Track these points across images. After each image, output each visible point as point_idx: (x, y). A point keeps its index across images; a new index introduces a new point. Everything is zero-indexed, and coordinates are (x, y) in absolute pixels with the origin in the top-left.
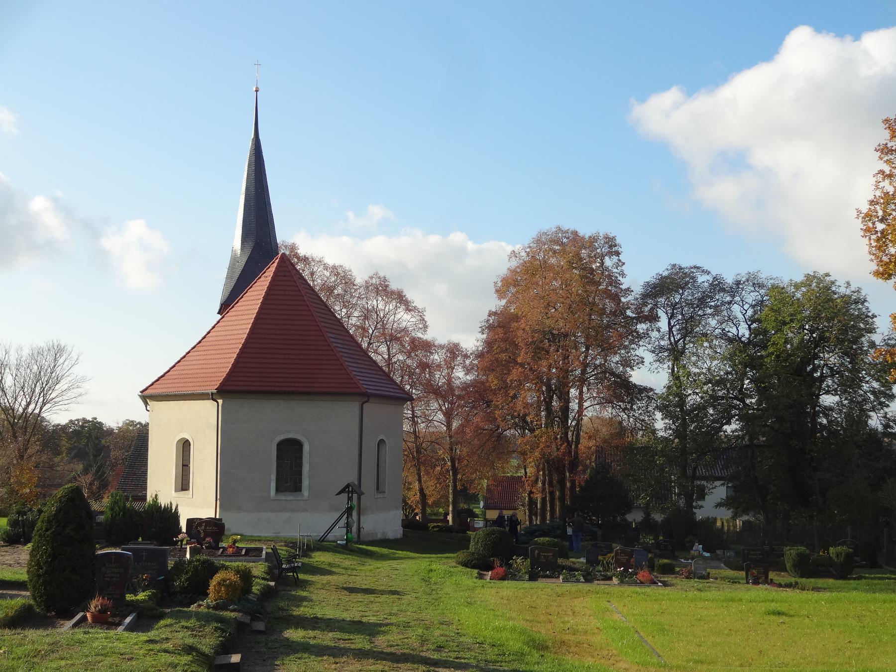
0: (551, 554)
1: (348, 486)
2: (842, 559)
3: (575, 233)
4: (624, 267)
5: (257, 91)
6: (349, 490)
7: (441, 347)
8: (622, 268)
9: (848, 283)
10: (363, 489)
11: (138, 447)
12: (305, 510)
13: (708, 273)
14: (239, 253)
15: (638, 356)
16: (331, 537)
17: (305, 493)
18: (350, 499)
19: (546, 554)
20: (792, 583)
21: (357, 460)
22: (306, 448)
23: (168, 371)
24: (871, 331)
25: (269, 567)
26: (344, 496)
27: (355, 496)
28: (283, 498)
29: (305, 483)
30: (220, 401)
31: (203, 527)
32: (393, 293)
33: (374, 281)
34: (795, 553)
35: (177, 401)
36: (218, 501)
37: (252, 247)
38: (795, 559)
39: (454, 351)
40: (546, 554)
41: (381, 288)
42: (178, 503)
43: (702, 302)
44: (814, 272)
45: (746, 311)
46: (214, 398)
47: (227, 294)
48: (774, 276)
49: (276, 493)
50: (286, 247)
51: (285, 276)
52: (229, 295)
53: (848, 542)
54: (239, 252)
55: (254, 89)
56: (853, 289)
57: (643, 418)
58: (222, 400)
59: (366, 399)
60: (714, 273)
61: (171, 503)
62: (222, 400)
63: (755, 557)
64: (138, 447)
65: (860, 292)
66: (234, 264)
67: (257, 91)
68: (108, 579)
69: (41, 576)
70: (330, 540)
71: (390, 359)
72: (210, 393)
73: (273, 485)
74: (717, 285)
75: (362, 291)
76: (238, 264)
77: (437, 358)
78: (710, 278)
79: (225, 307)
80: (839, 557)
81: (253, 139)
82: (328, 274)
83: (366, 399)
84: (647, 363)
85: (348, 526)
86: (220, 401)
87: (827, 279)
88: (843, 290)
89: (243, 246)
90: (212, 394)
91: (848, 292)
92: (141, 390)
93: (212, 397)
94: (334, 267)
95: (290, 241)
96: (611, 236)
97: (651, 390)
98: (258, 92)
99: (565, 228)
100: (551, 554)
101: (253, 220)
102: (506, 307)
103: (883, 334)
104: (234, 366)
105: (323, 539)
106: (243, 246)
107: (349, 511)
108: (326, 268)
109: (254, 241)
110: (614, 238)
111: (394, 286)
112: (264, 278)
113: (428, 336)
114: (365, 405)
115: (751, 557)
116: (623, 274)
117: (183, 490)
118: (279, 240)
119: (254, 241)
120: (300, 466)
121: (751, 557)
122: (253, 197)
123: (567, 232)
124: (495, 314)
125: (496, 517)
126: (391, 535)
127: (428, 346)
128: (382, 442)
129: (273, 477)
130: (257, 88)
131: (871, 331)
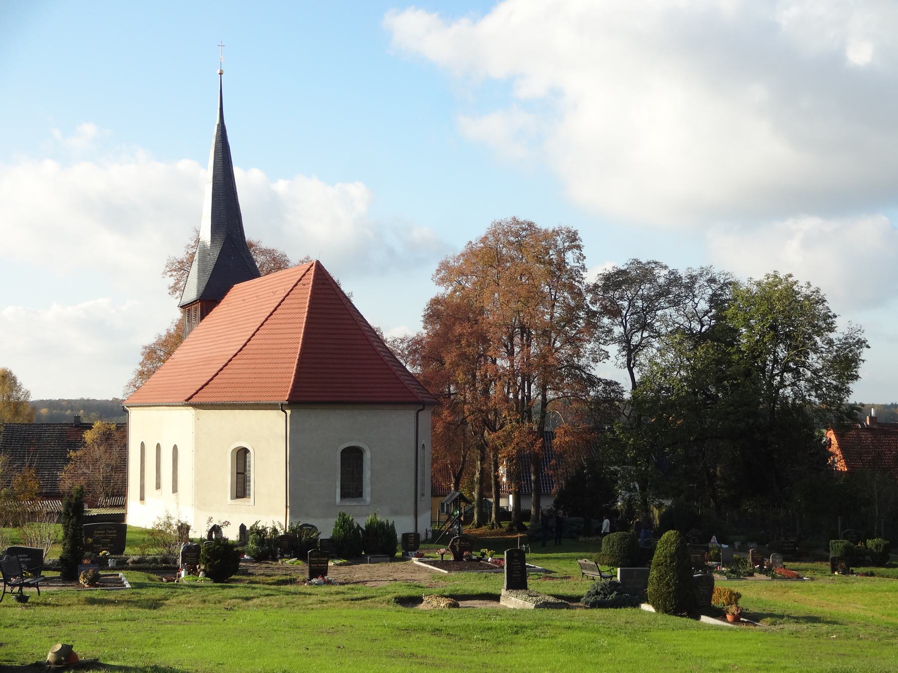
0: (700, 555)
2: (881, 550)
3: (531, 225)
4: (585, 262)
5: (221, 74)
8: (584, 262)
9: (809, 283)
11: (7, 439)
13: (666, 267)
14: (209, 245)
15: (603, 350)
19: (695, 556)
20: (868, 572)
22: (367, 456)
23: (212, 379)
24: (831, 330)
28: (348, 504)
29: (367, 489)
30: (288, 412)
31: (458, 542)
34: (842, 546)
35: (209, 410)
36: (288, 508)
37: (224, 240)
38: (843, 550)
40: (695, 556)
42: (173, 496)
43: (663, 292)
44: (775, 272)
45: (697, 304)
46: (283, 408)
47: (202, 288)
48: (726, 272)
49: (341, 500)
51: (323, 284)
52: (205, 289)
53: (852, 532)
54: (209, 243)
55: (219, 72)
56: (812, 289)
57: (609, 411)
58: (290, 411)
59: (421, 407)
60: (671, 268)
61: (387, 520)
62: (290, 411)
63: (788, 548)
64: (7, 439)
65: (818, 292)
66: (204, 257)
67: (221, 74)
68: (702, 593)
69: (671, 592)
72: (280, 404)
73: (338, 491)
74: (674, 280)
76: (209, 257)
78: (666, 272)
80: (878, 548)
81: (218, 125)
83: (421, 407)
84: (612, 358)
86: (288, 412)
87: (790, 279)
88: (805, 291)
89: (213, 238)
90: (282, 405)
91: (808, 293)
92: (186, 398)
93: (282, 408)
96: (573, 230)
97: (616, 383)
98: (222, 75)
99: (521, 220)
100: (700, 555)
101: (224, 211)
102: (451, 296)
103: (843, 333)
106: (213, 238)
109: (225, 233)
110: (575, 233)
112: (302, 286)
114: (420, 413)
115: (784, 548)
116: (584, 268)
117: (237, 497)
119: (225, 233)
121: (784, 548)
122: (221, 187)
123: (522, 223)
125: (34, 397)
129: (338, 484)
130: (221, 70)
131: (831, 330)
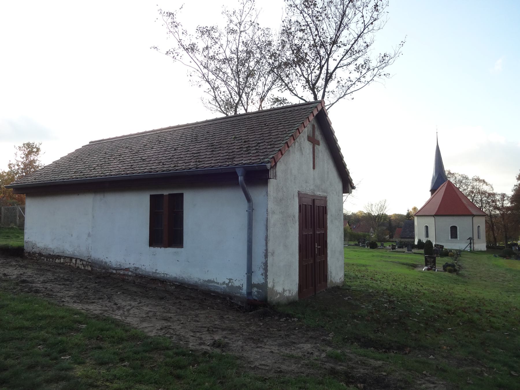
1: (470, 238)
6: (470, 239)
7: (499, 194)
10: (474, 238)
12: (459, 243)
16: (466, 249)
17: (458, 238)
18: (471, 241)
21: (472, 227)
22: (458, 228)
25: (297, 301)
26: (469, 240)
27: (472, 240)
29: (458, 236)
32: (481, 180)
33: (475, 178)
39: (503, 195)
41: (478, 180)
50: (447, 171)
70: (313, 96)
71: (481, 199)
73: (450, 237)
75: (471, 181)
77: (498, 198)
79: (433, 191)
82: (460, 177)
85: (471, 247)
94: (462, 175)
95: (448, 170)
104: (438, 209)
105: (464, 250)
107: (470, 243)
108: (459, 175)
111: (481, 178)
113: (495, 191)
118: (445, 169)
120: (457, 232)
124: (517, 186)
126: (483, 250)
127: (494, 194)
128: (479, 226)
129: (450, 235)
